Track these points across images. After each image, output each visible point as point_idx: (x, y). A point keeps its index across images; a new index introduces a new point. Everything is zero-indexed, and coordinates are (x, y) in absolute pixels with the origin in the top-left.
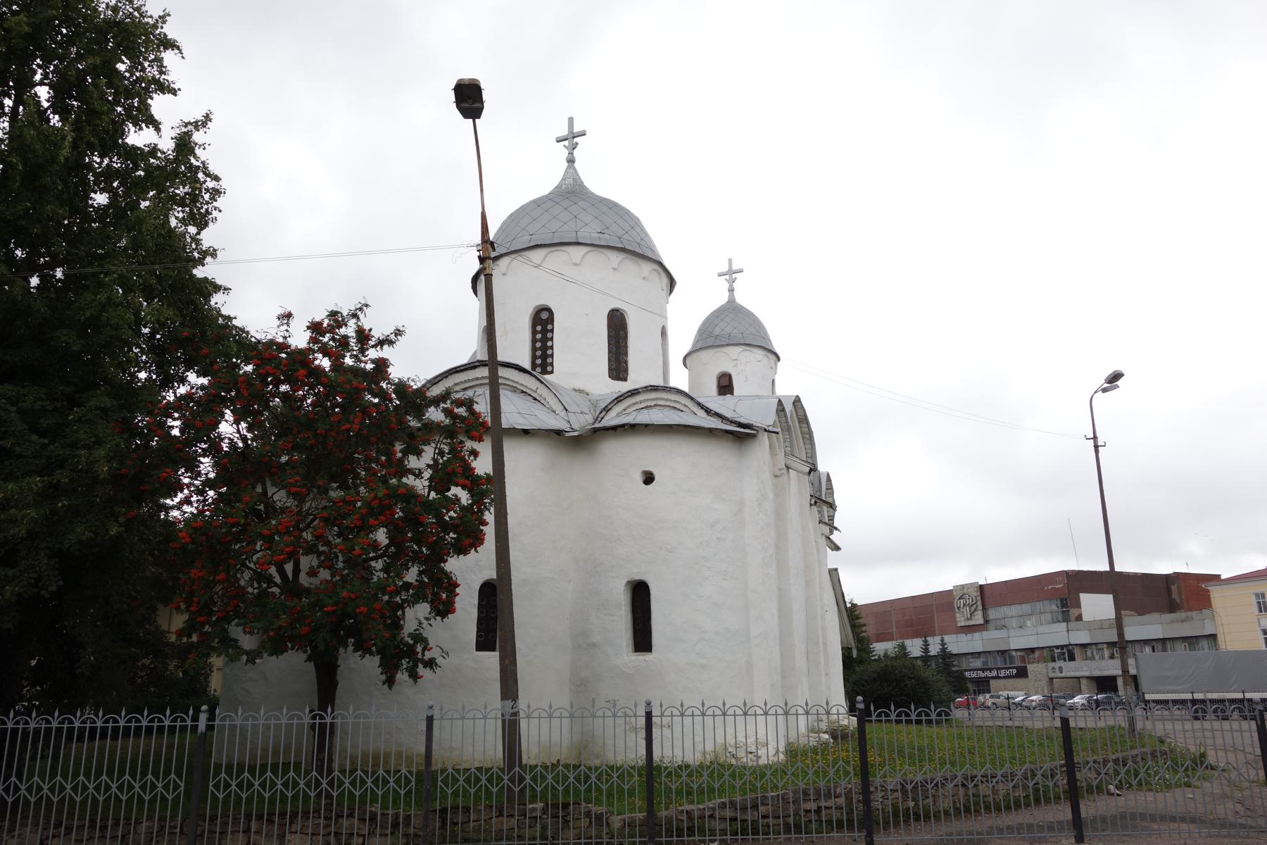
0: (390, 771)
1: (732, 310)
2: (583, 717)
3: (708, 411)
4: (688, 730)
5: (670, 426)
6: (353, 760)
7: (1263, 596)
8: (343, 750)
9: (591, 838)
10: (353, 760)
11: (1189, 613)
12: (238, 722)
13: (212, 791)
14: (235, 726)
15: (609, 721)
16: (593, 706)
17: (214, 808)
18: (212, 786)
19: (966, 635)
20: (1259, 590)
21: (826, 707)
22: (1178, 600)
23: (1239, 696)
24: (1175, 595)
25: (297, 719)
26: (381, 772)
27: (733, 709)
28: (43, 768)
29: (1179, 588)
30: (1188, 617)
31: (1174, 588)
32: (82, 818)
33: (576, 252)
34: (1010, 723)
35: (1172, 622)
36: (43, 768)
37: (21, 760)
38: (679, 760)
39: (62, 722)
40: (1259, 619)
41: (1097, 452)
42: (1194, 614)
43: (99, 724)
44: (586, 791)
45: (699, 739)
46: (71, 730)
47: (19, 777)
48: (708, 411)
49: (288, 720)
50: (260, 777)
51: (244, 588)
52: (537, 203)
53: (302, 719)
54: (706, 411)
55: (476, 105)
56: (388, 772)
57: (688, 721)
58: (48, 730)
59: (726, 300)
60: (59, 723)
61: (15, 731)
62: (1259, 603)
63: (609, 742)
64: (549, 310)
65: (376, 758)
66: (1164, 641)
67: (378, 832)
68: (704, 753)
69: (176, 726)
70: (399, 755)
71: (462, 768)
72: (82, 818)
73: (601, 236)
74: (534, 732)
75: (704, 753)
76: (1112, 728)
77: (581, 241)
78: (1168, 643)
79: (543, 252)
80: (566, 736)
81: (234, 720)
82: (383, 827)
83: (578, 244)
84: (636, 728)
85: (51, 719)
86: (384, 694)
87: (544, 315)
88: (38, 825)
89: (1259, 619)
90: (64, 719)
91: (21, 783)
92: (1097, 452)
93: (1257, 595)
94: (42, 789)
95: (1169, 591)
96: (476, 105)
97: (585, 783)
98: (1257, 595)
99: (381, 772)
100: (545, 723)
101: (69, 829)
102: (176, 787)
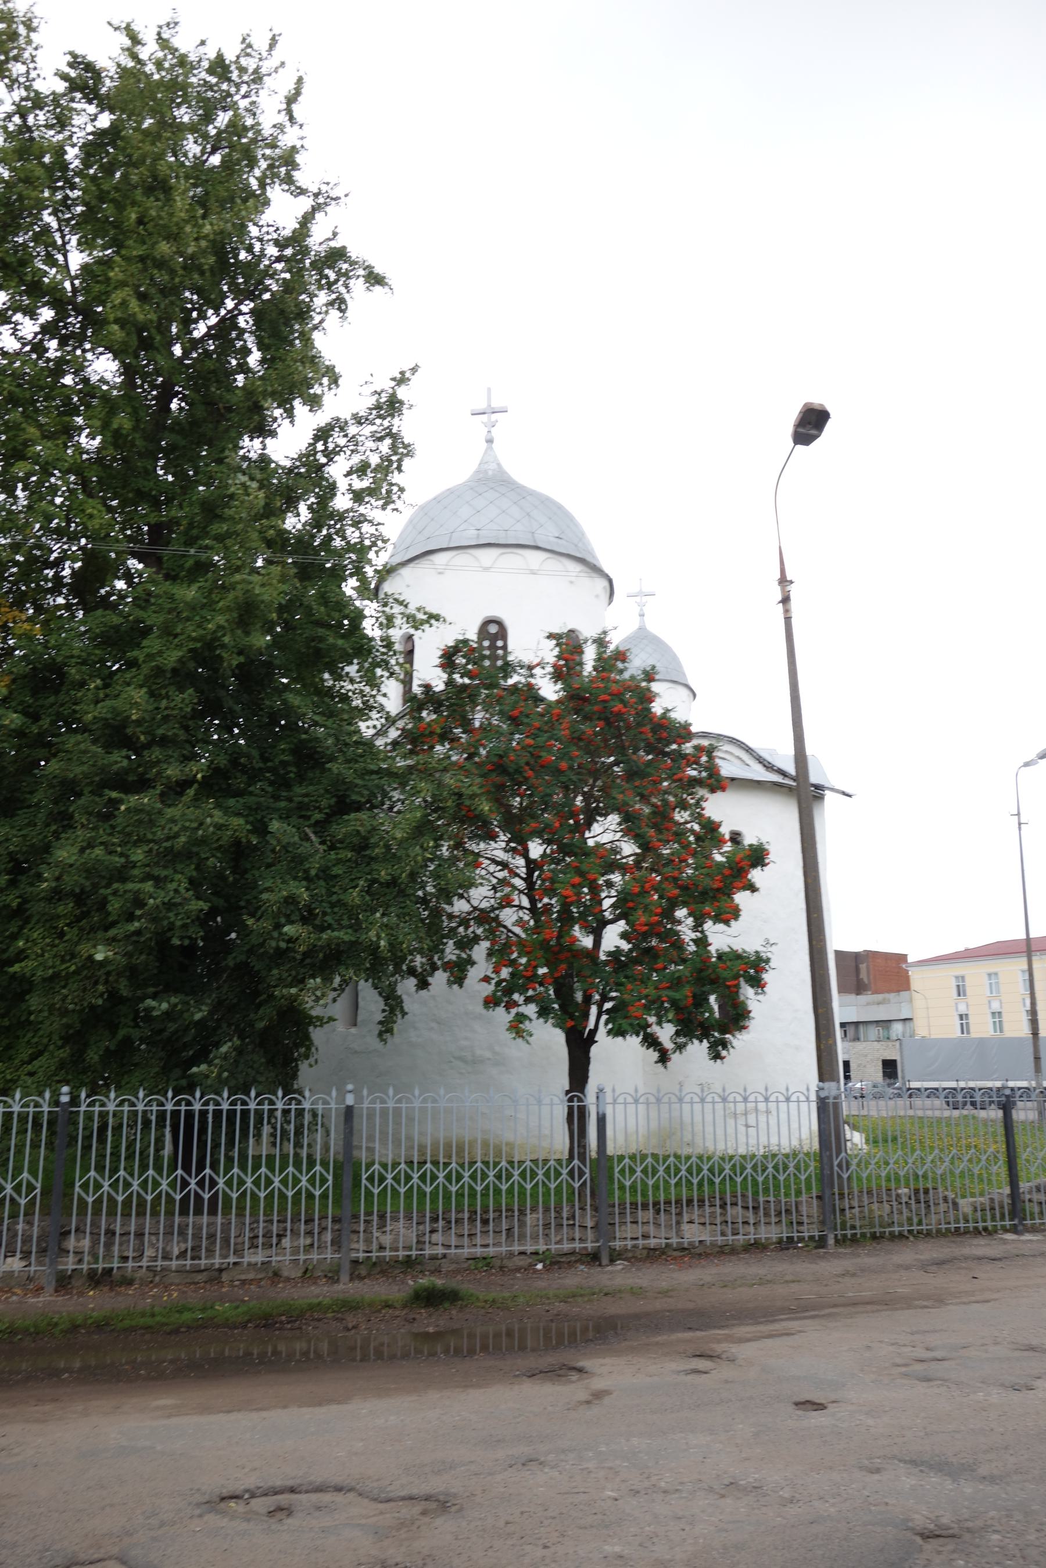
0: (439, 1163)
1: (642, 629)
2: (798, 1101)
3: (760, 760)
4: (783, 1116)
5: (758, 782)
6: (422, 1149)
7: (963, 978)
8: (409, 1138)
9: (949, 1223)
10: (422, 1149)
11: (886, 995)
12: (391, 1104)
13: (366, 1186)
14: (221, 1111)
15: (697, 1107)
16: (681, 1090)
17: (841, 1188)
18: (80, 1186)
19: (750, 1012)
20: (959, 973)
21: (742, 1093)
22: (866, 980)
23: (953, 1084)
24: (863, 975)
25: (158, 1105)
26: (504, 1164)
27: (754, 1095)
28: (101, 1156)
29: (868, 967)
30: (884, 999)
31: (863, 967)
32: (460, 1210)
33: (535, 558)
34: (911, 1113)
35: (868, 1004)
36: (101, 1156)
37: (202, 1144)
38: (742, 1151)
39: (373, 1102)
40: (989, 1002)
41: (1020, 829)
42: (892, 996)
43: (252, 1106)
44: (676, 1184)
45: (794, 1125)
46: (245, 1113)
47: (214, 1167)
48: (760, 760)
49: (174, 1105)
50: (281, 1173)
51: (181, 945)
52: (451, 492)
53: (329, 1104)
54: (765, 766)
55: (801, 430)
56: (462, 1166)
57: (793, 1106)
58: (189, 1114)
59: (636, 627)
60: (258, 1104)
61: (203, 1114)
62: (958, 986)
63: (698, 1128)
64: (499, 623)
65: (448, 1146)
66: (857, 1024)
67: (763, 1221)
68: (800, 1140)
69: (235, 1110)
70: (486, 1144)
71: (541, 1158)
72: (460, 1210)
73: (559, 541)
74: (620, 1118)
75: (800, 1140)
76: (893, 1117)
77: (540, 545)
78: (861, 1028)
79: (494, 552)
80: (642, 1122)
81: (163, 1105)
82: (767, 1214)
83: (537, 548)
84: (735, 1114)
85: (133, 1099)
86: (461, 1073)
87: (493, 629)
88: (411, 1219)
89: (989, 1002)
90: (123, 1101)
91: (190, 1176)
92: (1020, 829)
93: (957, 977)
94: (412, 1178)
95: (857, 970)
96: (814, 432)
97: (698, 1175)
98: (957, 977)
99: (504, 1164)
100: (697, 1107)
101: (485, 1222)
102: (31, 1188)
